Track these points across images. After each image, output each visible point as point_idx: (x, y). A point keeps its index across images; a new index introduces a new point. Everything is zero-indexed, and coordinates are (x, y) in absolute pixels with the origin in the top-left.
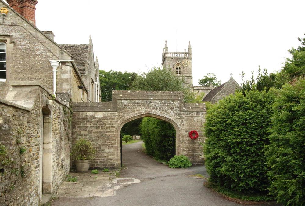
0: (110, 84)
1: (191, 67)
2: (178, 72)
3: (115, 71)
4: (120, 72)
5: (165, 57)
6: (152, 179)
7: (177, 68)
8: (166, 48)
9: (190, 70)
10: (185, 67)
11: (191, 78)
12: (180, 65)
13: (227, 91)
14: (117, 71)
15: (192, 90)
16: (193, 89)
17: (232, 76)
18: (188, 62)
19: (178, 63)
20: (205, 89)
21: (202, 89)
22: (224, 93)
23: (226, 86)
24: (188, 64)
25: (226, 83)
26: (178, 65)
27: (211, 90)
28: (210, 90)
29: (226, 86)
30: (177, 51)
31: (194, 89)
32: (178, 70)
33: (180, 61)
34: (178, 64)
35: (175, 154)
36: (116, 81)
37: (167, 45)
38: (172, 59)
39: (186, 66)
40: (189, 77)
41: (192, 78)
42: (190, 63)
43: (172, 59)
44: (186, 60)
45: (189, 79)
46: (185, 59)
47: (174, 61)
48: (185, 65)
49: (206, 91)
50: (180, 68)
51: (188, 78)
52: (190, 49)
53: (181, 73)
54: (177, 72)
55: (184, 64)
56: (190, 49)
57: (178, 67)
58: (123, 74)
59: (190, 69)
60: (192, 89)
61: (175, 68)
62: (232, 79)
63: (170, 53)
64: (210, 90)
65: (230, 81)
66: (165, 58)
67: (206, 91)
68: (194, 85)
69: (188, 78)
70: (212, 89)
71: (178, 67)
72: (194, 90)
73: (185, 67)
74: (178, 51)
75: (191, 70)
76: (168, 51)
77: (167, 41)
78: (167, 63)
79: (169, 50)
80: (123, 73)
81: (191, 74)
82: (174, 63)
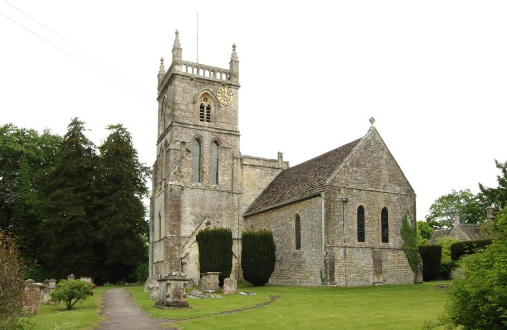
0: (7, 154)
1: (237, 107)
2: (205, 116)
3: (19, 128)
4: (32, 132)
5: (175, 72)
6: (230, 312)
7: (202, 107)
8: (177, 49)
9: (233, 114)
10: (223, 106)
11: (237, 135)
12: (209, 100)
13: (363, 163)
14: (24, 129)
15: (240, 166)
16: (241, 162)
17: (374, 125)
18: (231, 94)
19: (207, 93)
20: (268, 165)
21: (262, 165)
22: (355, 168)
23: (362, 151)
24: (231, 100)
25: (358, 141)
26: (206, 100)
27: (280, 171)
28: (278, 169)
29: (362, 151)
30: (199, 63)
31: (245, 162)
32: (205, 113)
33: (212, 90)
34: (206, 97)
35: (274, 270)
36: (20, 148)
37: (180, 42)
38: (192, 79)
39: (226, 103)
40: (233, 133)
41: (239, 135)
42: (236, 98)
43: (192, 79)
44: (226, 89)
45: (233, 138)
46: (223, 85)
47: (195, 86)
48: (222, 101)
49: (270, 172)
50: (209, 108)
51: (231, 134)
52: (234, 62)
53: (211, 120)
54: (202, 117)
55: (220, 98)
56: (234, 62)
57: (206, 104)
58: (40, 136)
59: (235, 112)
60: (239, 163)
61: (198, 105)
62: (374, 132)
63: (188, 65)
64: (278, 169)
65: (370, 138)
66: (173, 74)
67: (270, 172)
68: (243, 154)
69: (231, 134)
70: (285, 169)
71: (206, 104)
72: (242, 165)
73: (223, 106)
74: (201, 62)
75: (236, 115)
76: (181, 57)
77: (179, 31)
78: (179, 89)
79: (186, 56)
80: (41, 133)
81: (237, 125)
82: (195, 91)
